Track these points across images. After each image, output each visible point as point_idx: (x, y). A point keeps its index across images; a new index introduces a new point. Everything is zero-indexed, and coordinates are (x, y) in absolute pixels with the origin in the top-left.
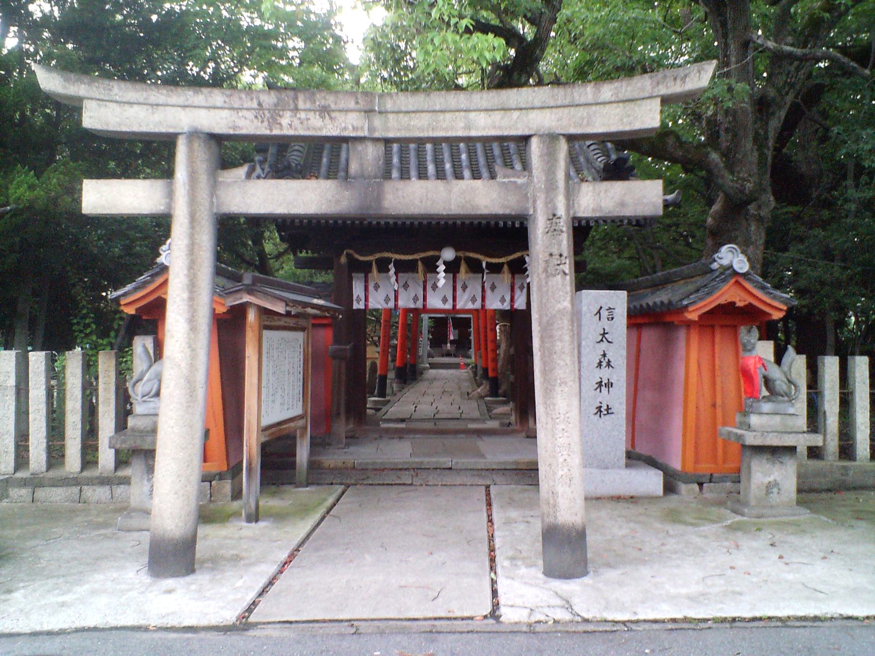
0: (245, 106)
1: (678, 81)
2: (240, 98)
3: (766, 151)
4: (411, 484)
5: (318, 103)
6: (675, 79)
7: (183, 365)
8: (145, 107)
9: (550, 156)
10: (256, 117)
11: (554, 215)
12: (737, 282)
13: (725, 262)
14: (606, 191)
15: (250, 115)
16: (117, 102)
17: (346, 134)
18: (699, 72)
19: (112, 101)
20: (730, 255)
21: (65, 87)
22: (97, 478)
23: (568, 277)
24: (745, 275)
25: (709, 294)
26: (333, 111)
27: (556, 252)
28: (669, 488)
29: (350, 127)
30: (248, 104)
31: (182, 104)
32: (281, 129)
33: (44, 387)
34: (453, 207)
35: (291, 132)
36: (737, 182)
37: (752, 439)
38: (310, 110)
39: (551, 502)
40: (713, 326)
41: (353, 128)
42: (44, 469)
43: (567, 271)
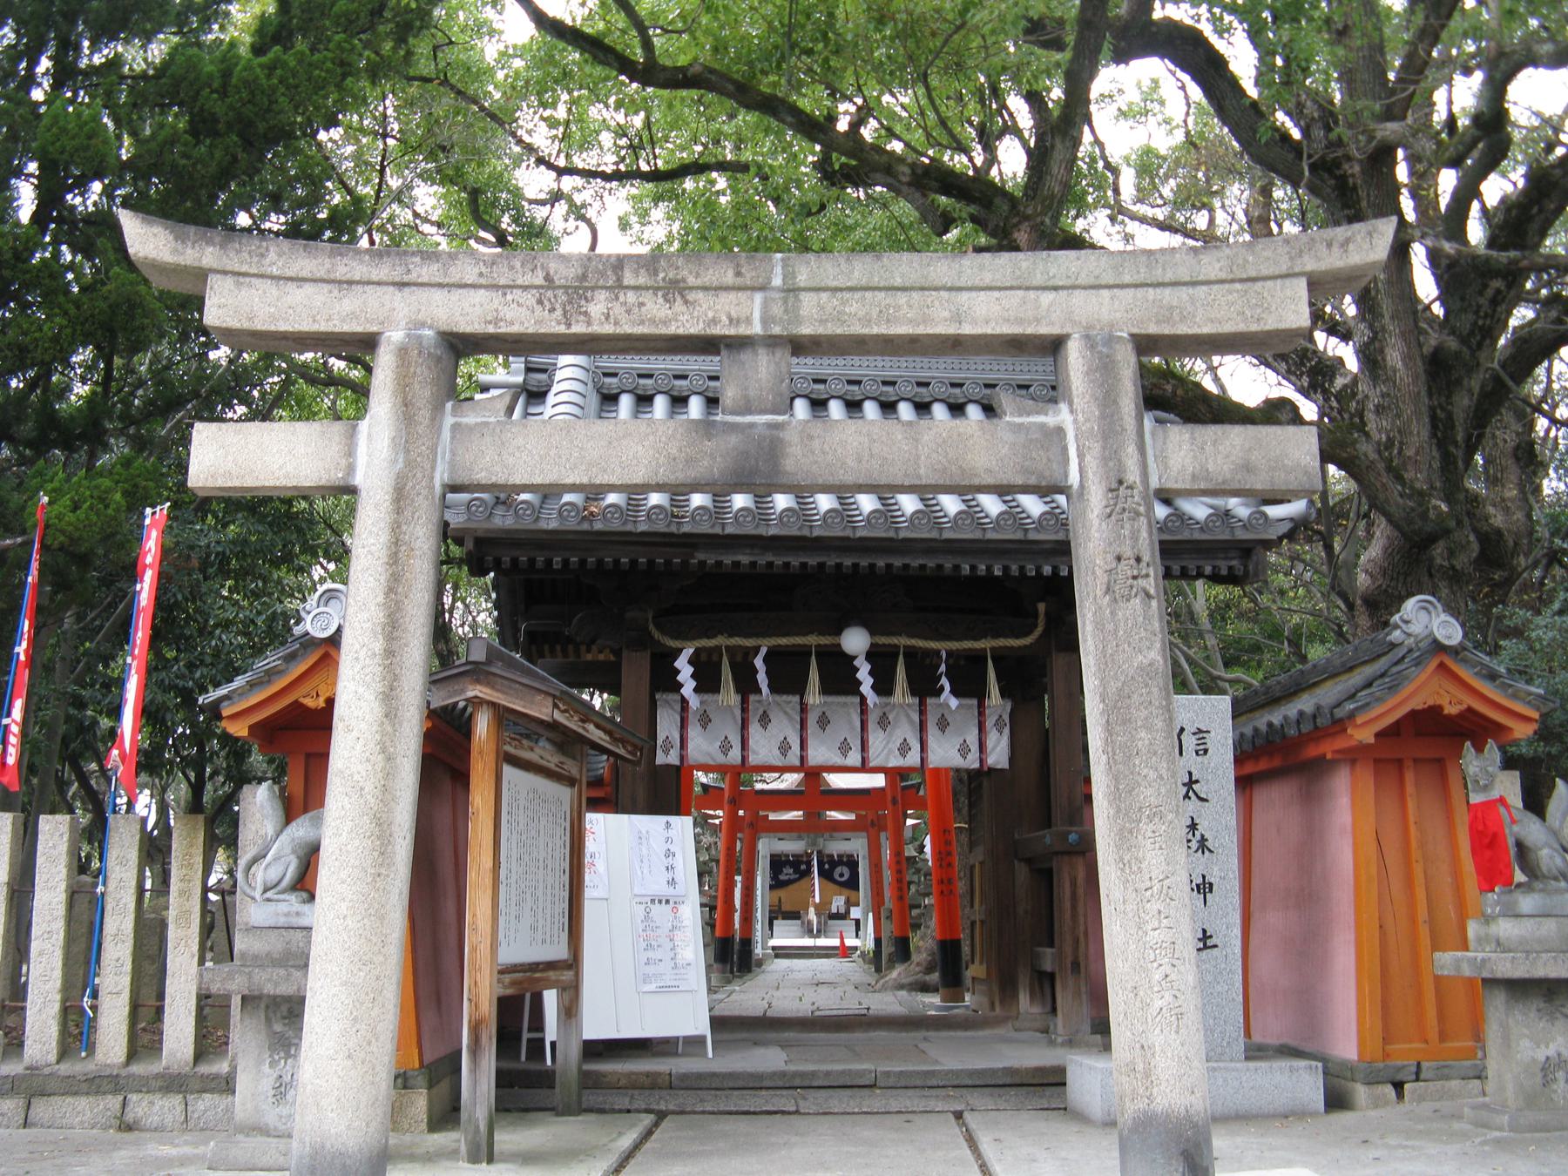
0: (519, 282)
1: (1335, 249)
2: (512, 268)
3: (1452, 449)
4: (797, 1112)
5: (662, 275)
6: (1329, 245)
7: (369, 787)
8: (326, 287)
9: (1104, 368)
10: (540, 302)
11: (1120, 482)
12: (1442, 666)
13: (1417, 628)
14: (1215, 443)
15: (529, 298)
16: (272, 277)
17: (717, 331)
18: (1370, 234)
19: (262, 276)
20: (1423, 615)
21: (175, 251)
22: (157, 1076)
23: (1154, 603)
24: (1455, 651)
25: (1393, 689)
26: (691, 288)
27: (1128, 552)
28: (1336, 1101)
29: (724, 318)
30: (528, 279)
31: (397, 279)
32: (589, 324)
33: (63, 886)
34: (922, 471)
35: (608, 329)
36: (1410, 497)
37: (1508, 965)
38: (647, 288)
39: (1140, 1067)
40: (1399, 762)
41: (731, 320)
42: (53, 1057)
43: (1152, 591)
